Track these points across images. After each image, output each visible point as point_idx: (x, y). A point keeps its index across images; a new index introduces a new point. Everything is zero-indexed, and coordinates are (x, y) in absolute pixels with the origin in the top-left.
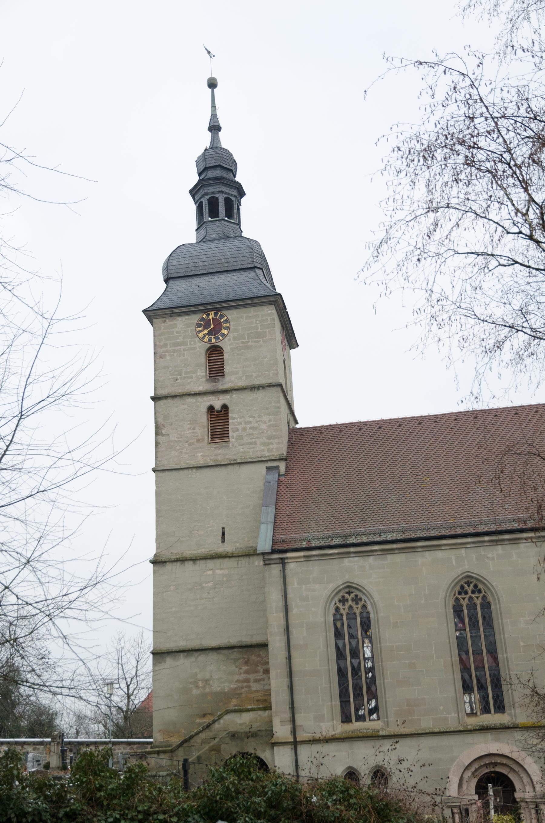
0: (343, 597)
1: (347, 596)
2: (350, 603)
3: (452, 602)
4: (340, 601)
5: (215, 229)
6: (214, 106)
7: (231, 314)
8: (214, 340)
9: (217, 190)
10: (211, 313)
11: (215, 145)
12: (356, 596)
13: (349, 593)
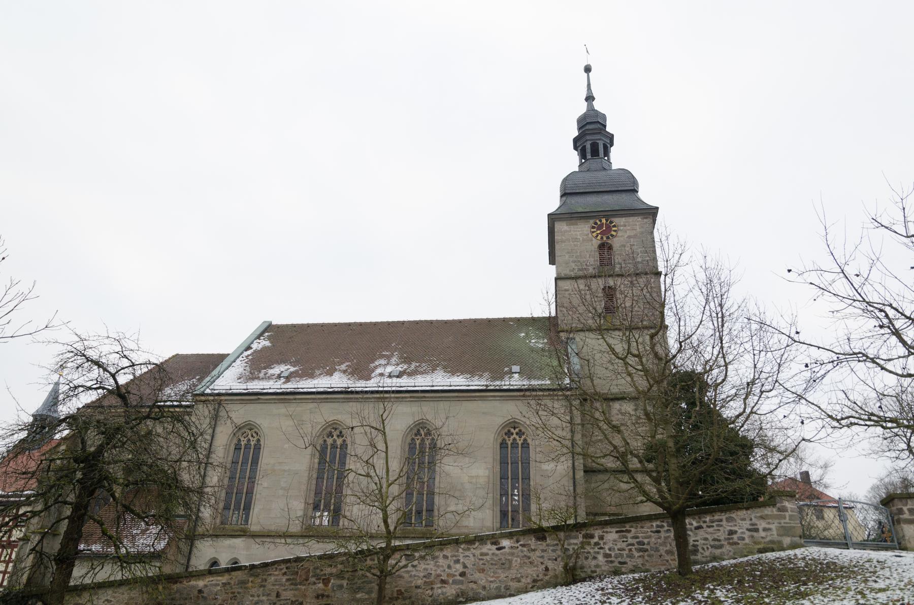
0: (509, 431)
1: (512, 430)
2: (515, 436)
3: (409, 440)
4: (506, 434)
5: (594, 163)
6: (589, 85)
7: (617, 221)
8: (605, 239)
9: (593, 137)
10: (603, 221)
11: (591, 110)
12: (520, 431)
13: (515, 428)
